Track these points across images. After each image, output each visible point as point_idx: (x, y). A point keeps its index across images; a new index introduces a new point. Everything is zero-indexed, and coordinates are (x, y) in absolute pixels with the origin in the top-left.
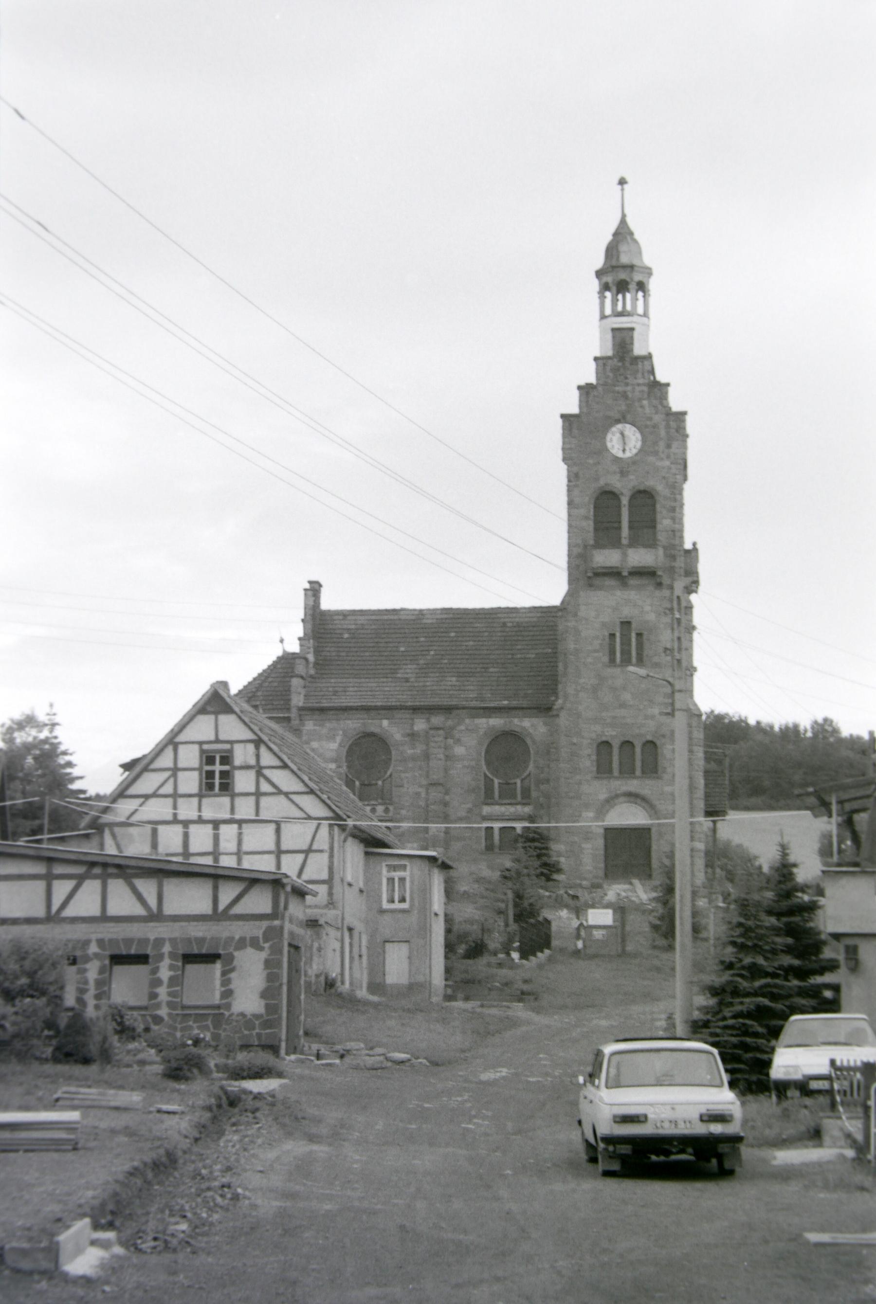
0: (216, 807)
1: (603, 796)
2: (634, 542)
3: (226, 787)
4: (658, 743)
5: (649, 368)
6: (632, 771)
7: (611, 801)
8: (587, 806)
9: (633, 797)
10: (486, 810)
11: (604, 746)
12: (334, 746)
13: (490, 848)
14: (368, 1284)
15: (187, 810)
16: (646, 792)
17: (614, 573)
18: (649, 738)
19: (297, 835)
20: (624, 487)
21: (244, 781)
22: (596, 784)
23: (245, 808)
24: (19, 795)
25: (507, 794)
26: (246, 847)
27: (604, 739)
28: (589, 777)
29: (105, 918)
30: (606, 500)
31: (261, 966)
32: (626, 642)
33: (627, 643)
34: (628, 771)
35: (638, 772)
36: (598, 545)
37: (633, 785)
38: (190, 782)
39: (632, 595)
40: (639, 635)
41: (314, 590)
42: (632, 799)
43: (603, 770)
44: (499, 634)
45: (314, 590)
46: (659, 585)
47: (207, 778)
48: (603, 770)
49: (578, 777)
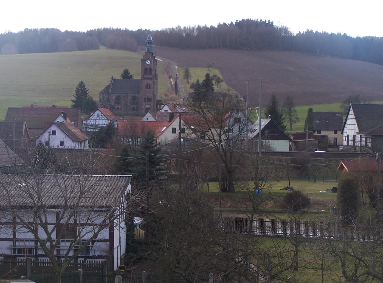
0: (98, 118)
1: (145, 104)
2: (149, 75)
3: (99, 117)
9: (149, 104)
10: (132, 105)
11: (145, 98)
12: (114, 97)
13: (132, 109)
14: (282, 178)
15: (96, 118)
17: (146, 78)
19: (104, 121)
20: (148, 68)
21: (100, 116)
23: (100, 118)
24: (105, 234)
25: (134, 103)
30: (146, 69)
32: (148, 86)
33: (148, 86)
34: (148, 101)
36: (145, 75)
38: (96, 116)
39: (149, 81)
40: (149, 86)
41: (112, 77)
43: (145, 101)
45: (112, 77)
46: (152, 80)
47: (63, 256)
48: (145, 101)
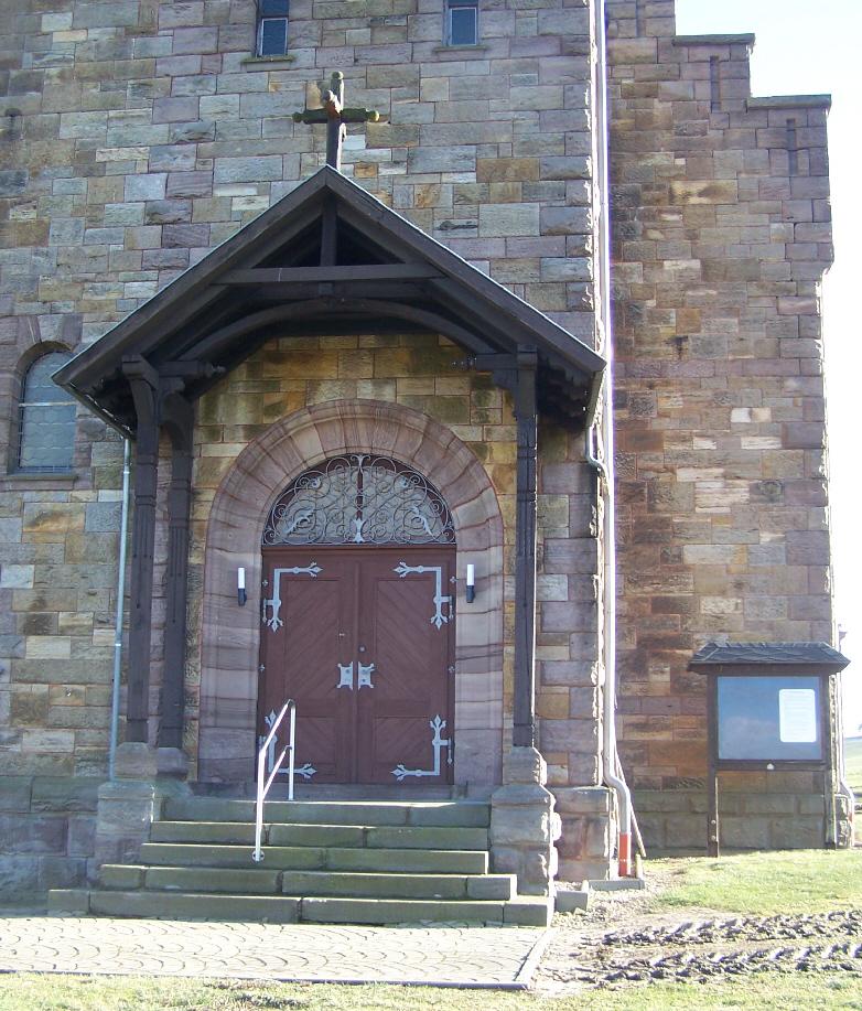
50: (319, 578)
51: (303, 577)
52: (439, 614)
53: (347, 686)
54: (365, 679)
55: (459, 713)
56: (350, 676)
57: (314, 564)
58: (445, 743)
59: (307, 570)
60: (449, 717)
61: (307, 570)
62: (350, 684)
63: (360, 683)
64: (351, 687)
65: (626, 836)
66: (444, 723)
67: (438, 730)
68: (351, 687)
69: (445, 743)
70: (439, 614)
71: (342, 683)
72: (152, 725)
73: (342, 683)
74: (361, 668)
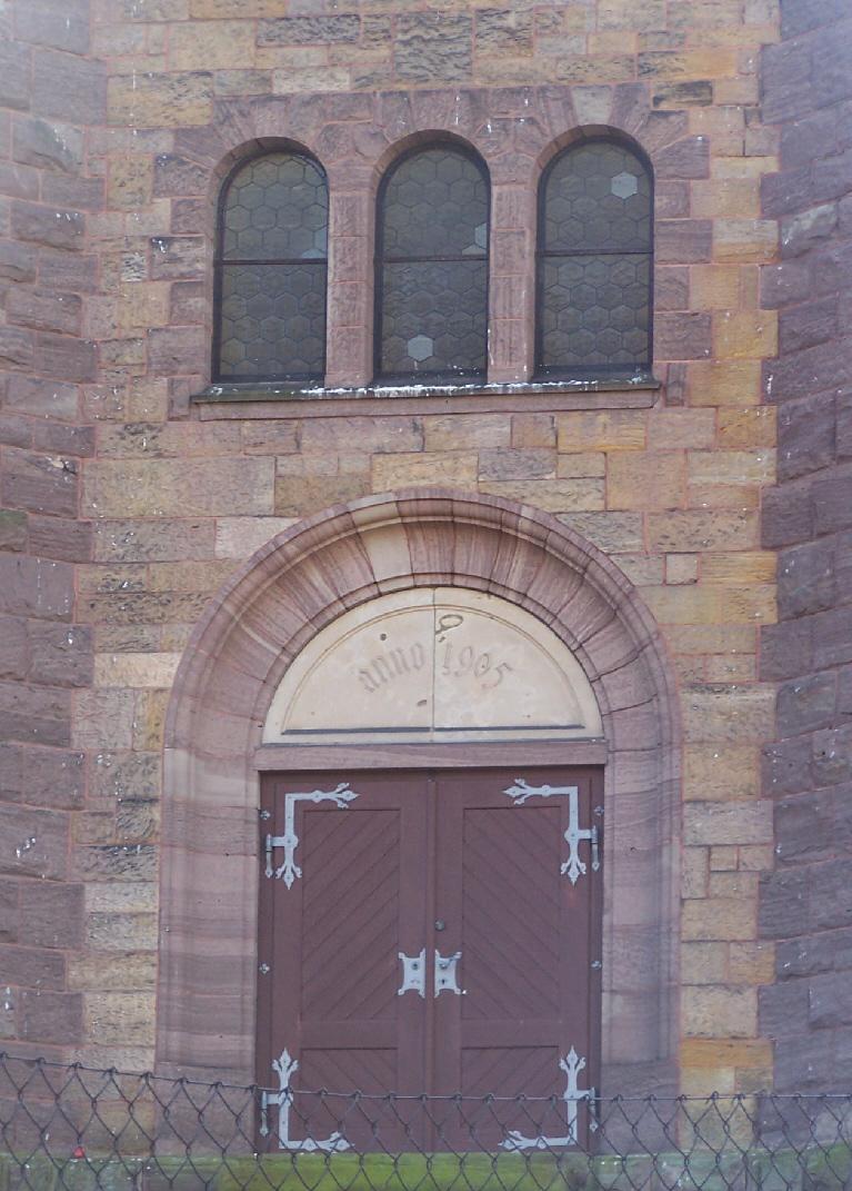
1: (241, 540)
4: (653, 142)
5: (320, 370)
6: (464, 364)
7: (306, 573)
8: (137, 609)
9: (469, 536)
16: (543, 498)
18: (596, 112)
22: (208, 444)
26: (449, 570)
27: (268, 125)
28: (150, 399)
29: (606, 511)
31: (755, 369)
35: (509, 369)
37: (462, 453)
42: (472, 556)
44: (301, 599)
48: (256, 355)
49: (67, 403)
50: (352, 807)
51: (328, 808)
52: (574, 857)
53: (416, 991)
54: (447, 979)
55: (611, 1027)
56: (420, 974)
57: (344, 785)
58: (586, 834)
59: (331, 796)
60: (592, 1052)
61: (331, 796)
62: (421, 987)
63: (438, 987)
64: (422, 993)
65: (59, 814)
66: (564, 870)
67: (289, 862)
68: (422, 993)
69: (586, 834)
70: (574, 857)
71: (407, 985)
72: (670, 1081)
73: (407, 985)
74: (439, 960)
